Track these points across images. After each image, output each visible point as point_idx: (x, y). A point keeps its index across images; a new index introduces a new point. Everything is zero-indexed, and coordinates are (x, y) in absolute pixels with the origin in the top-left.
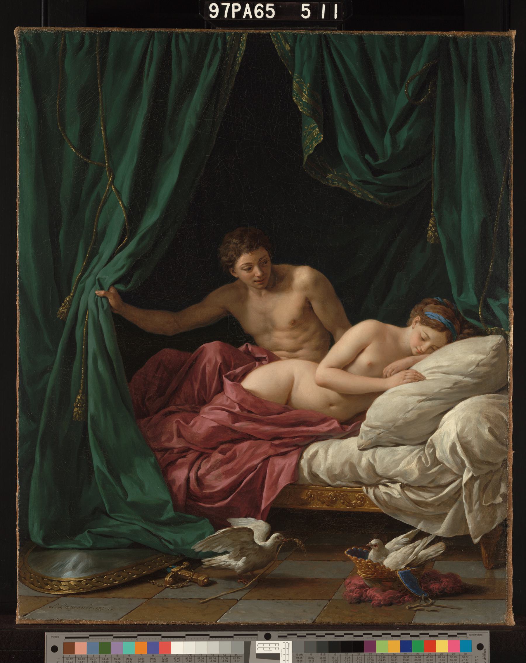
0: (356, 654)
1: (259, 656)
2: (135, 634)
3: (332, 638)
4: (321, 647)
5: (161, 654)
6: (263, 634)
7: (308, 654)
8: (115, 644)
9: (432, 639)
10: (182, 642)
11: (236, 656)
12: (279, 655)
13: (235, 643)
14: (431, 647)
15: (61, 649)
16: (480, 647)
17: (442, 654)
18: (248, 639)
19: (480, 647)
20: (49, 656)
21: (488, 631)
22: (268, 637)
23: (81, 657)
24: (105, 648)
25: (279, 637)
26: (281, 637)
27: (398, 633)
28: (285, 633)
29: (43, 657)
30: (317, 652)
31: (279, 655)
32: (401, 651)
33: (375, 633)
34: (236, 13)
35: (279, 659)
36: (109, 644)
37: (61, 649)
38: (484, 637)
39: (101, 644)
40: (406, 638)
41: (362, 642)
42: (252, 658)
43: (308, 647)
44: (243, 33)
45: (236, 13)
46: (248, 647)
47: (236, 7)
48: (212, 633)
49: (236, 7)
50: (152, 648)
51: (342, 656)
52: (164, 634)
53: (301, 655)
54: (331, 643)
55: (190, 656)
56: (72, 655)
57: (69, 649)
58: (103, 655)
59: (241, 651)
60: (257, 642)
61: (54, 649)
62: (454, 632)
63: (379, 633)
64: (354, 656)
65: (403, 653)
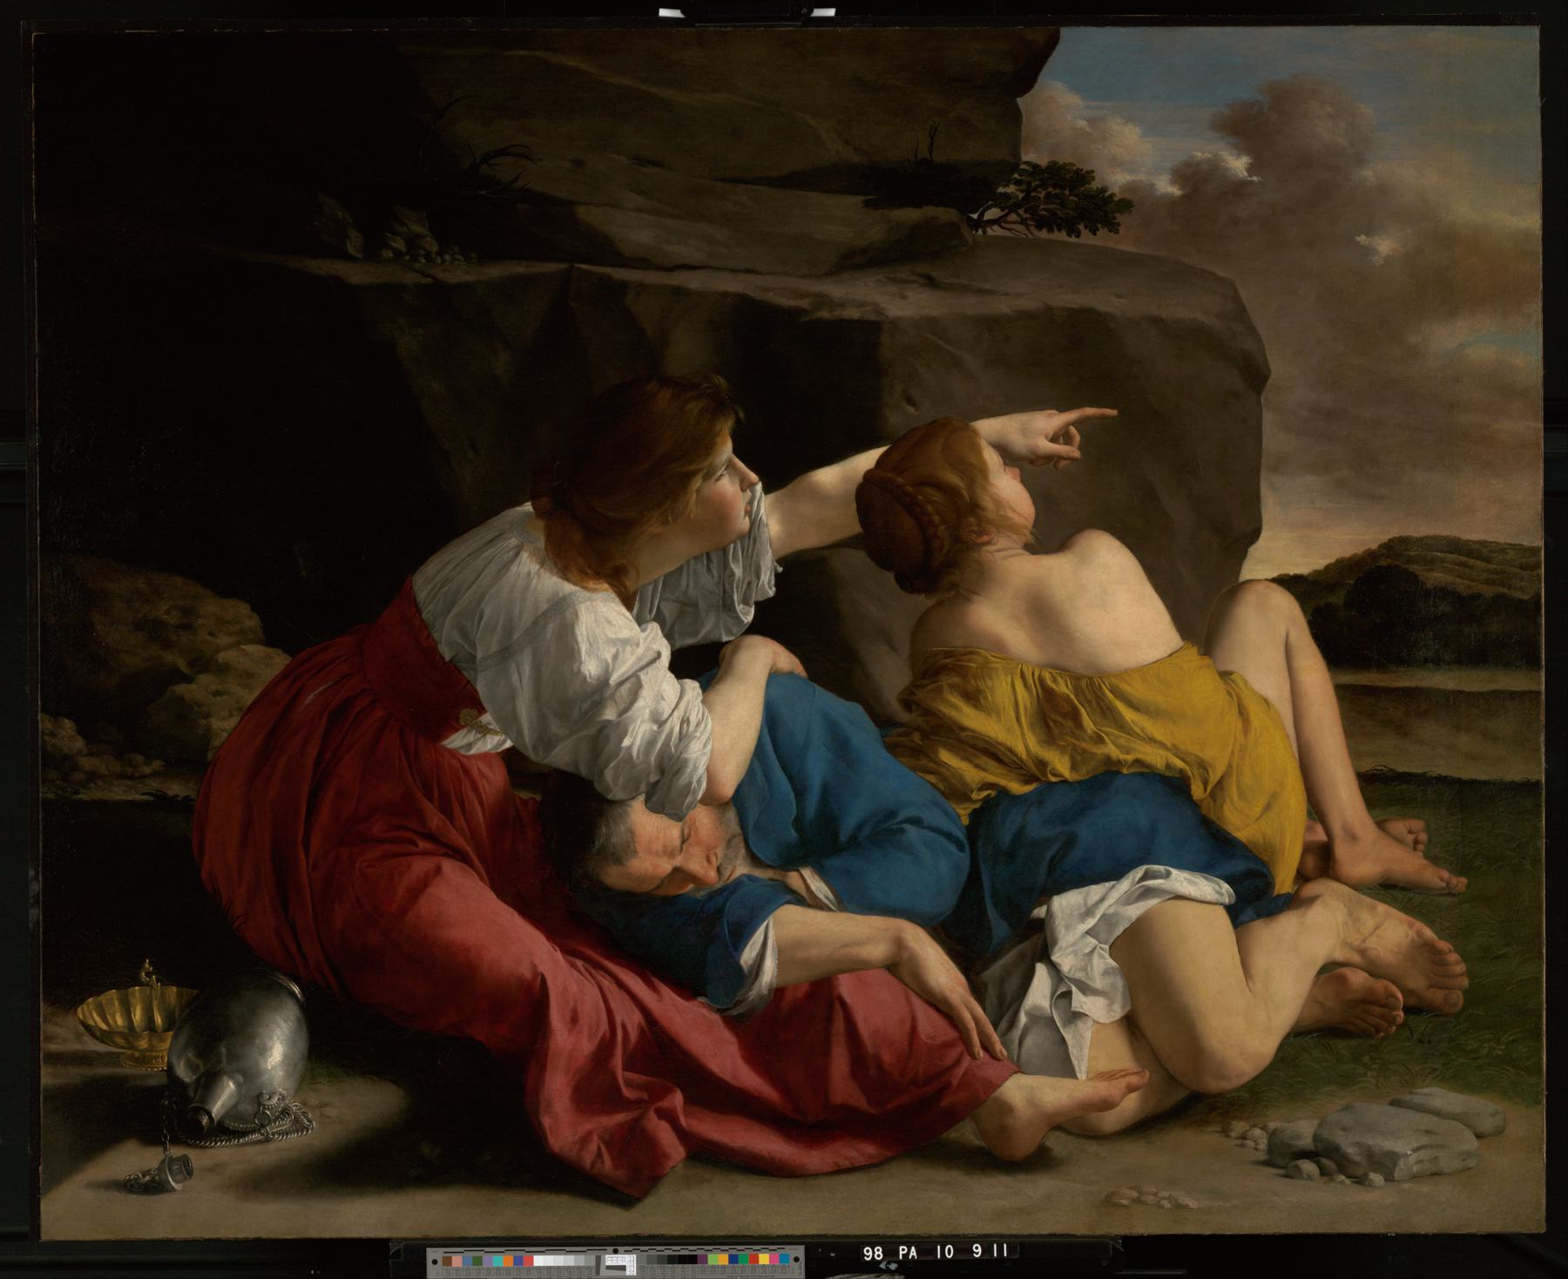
0: (680, 1266)
1: (609, 1268)
2: (584, 1249)
3: (670, 1253)
4: (661, 1260)
5: (484, 1266)
6: (611, 1249)
7: (650, 1266)
8: (485, 1257)
9: (756, 1253)
10: (552, 1256)
11: (589, 1268)
12: (625, 1266)
13: (506, 1257)
14: (755, 1259)
15: (440, 1262)
16: (796, 1259)
17: (764, 1266)
18: (598, 1253)
19: (796, 1259)
20: (431, 1271)
21: (803, 1246)
22: (616, 1252)
23: (457, 1269)
24: (478, 1261)
25: (626, 1251)
26: (627, 1252)
27: (726, 1247)
28: (630, 1248)
29: (425, 1273)
30: (658, 1263)
31: (625, 1266)
32: (730, 1263)
33: (707, 1248)
34: (903, 1255)
35: (625, 1270)
36: (481, 1258)
37: (440, 1262)
38: (800, 1251)
39: (474, 1257)
40: (734, 1252)
41: (696, 1256)
42: (604, 1273)
43: (650, 1260)
44: (1009, 456)
45: (903, 1255)
46: (598, 1260)
47: (903, 1250)
48: (568, 1249)
49: (903, 1250)
50: (518, 1261)
51: (679, 1267)
52: (486, 1249)
53: (644, 1267)
54: (669, 1256)
55: (550, 1267)
56: (449, 1267)
57: (447, 1261)
58: (476, 1267)
59: (594, 1264)
60: (607, 1256)
61: (435, 1262)
62: (775, 1247)
63: (710, 1248)
64: (689, 1267)
65: (731, 1265)
